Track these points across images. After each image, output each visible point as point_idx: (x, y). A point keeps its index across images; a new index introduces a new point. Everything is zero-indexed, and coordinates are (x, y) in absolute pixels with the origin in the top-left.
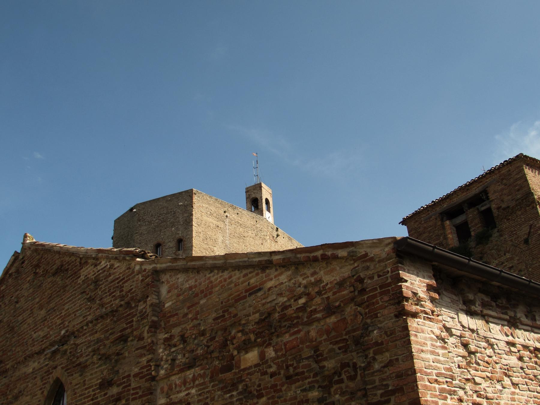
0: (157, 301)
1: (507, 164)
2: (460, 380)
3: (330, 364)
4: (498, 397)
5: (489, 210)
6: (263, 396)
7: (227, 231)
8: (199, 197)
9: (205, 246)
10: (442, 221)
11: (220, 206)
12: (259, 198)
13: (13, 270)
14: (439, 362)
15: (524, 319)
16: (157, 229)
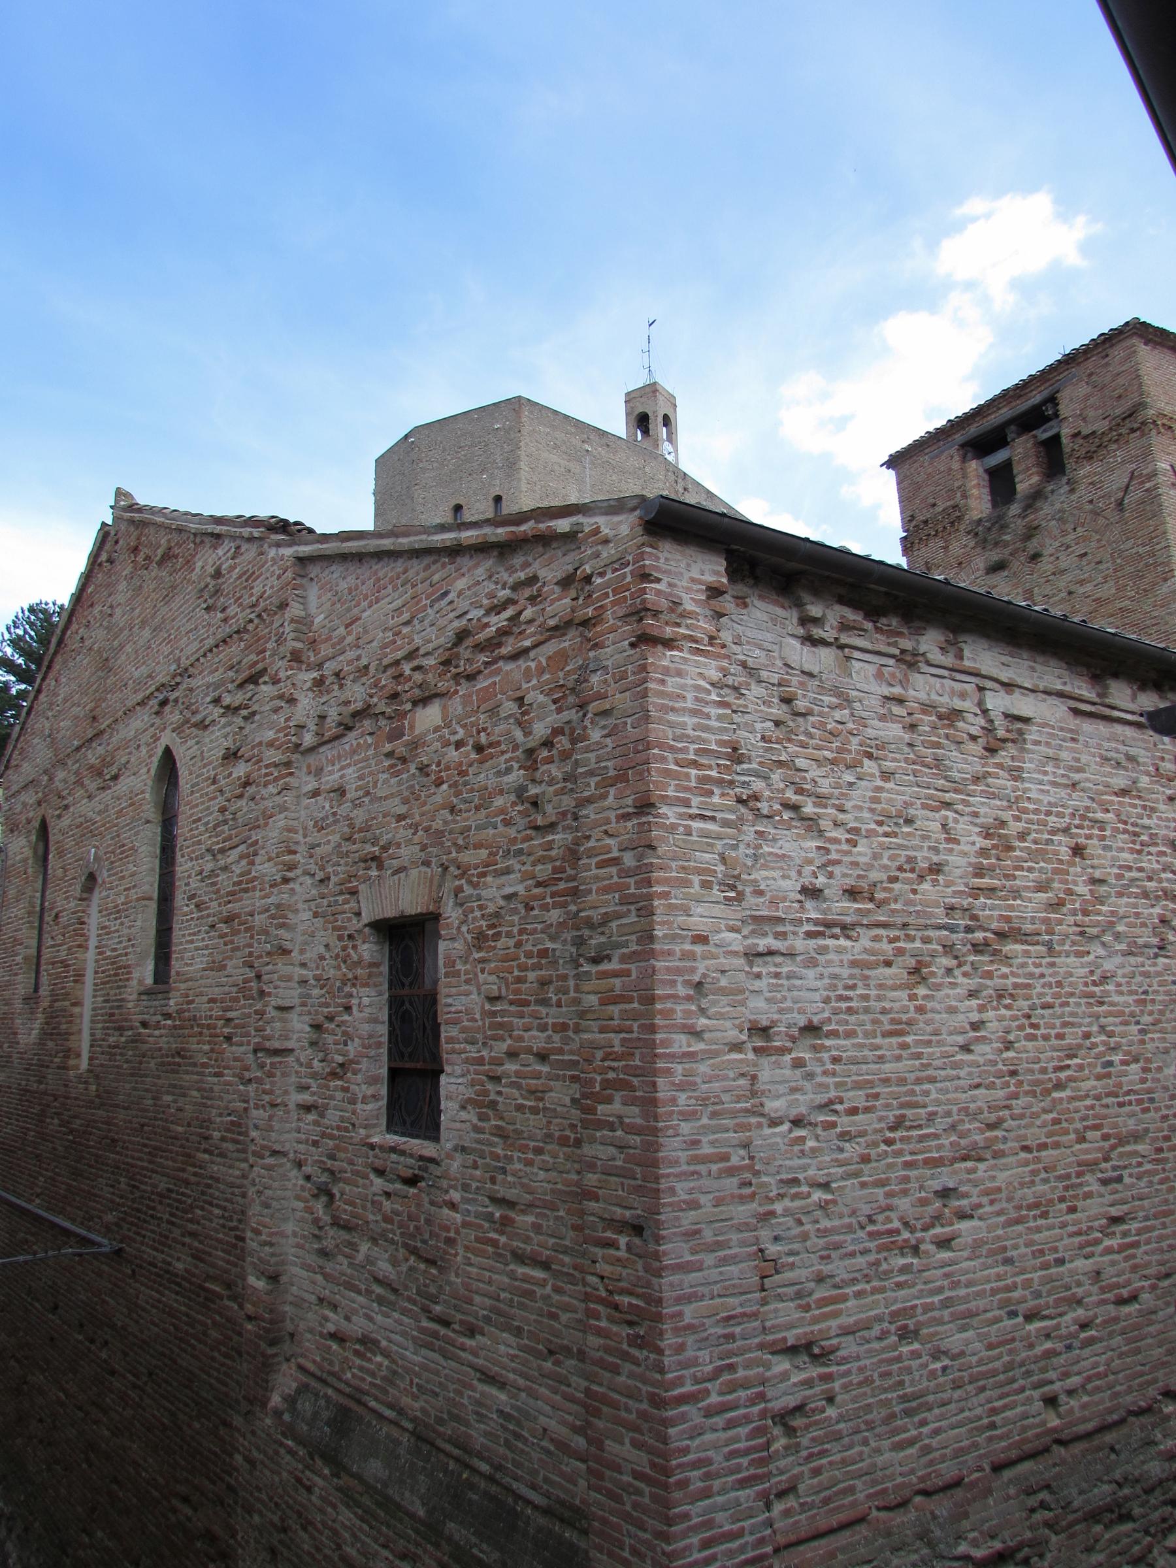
0: (303, 614)
1: (1104, 342)
2: (760, 763)
3: (540, 730)
4: (842, 794)
5: (1056, 438)
6: (443, 783)
10: (964, 459)
13: (104, 557)
14: (707, 729)
15: (936, 656)
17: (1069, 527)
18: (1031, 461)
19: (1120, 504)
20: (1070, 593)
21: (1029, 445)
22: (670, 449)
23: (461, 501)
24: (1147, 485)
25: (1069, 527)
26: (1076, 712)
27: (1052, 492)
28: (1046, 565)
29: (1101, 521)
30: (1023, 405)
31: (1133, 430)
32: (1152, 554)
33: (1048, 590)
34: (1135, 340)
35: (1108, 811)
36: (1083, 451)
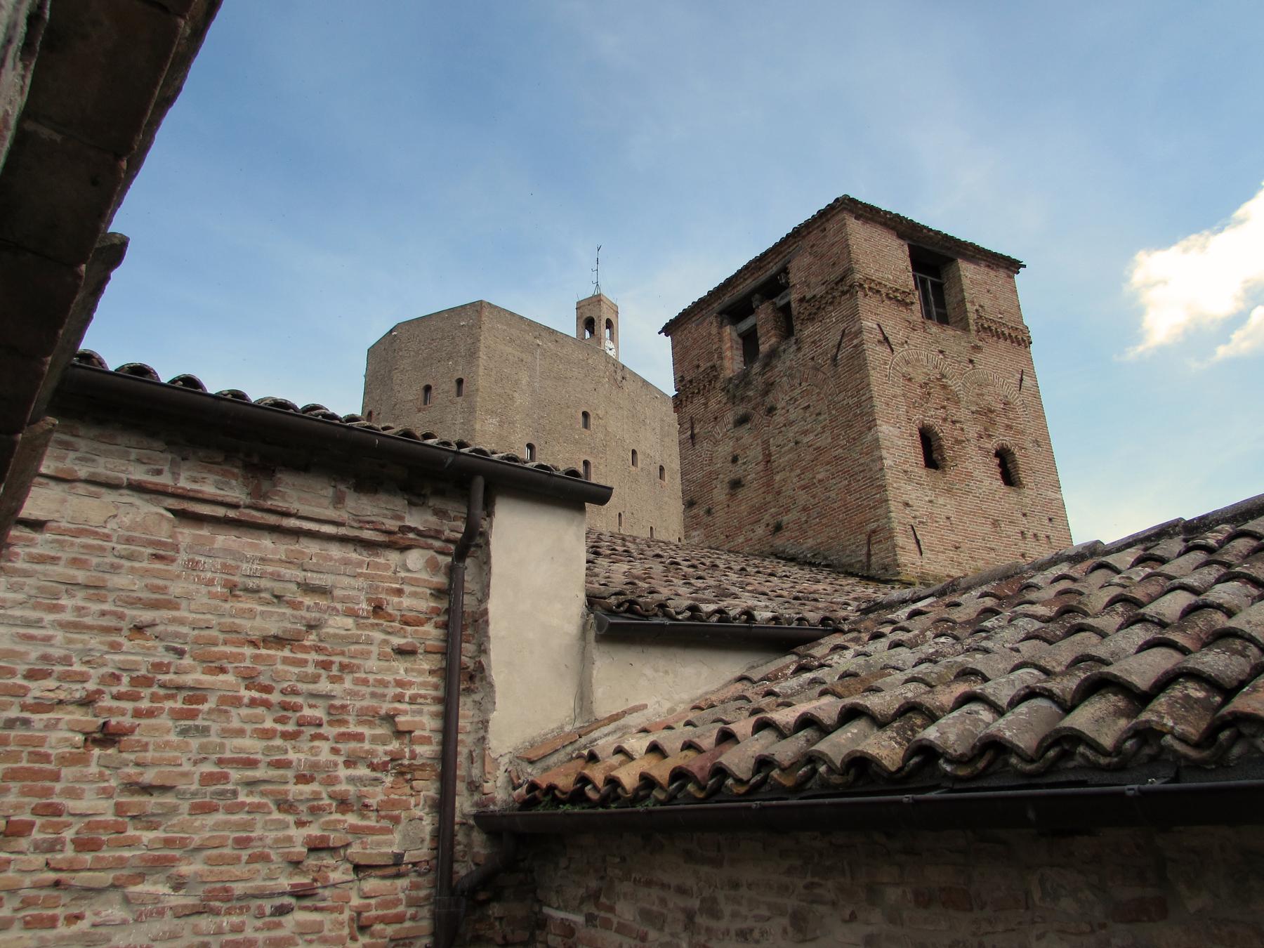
5: (788, 304)
7: (538, 368)
8: (492, 313)
9: (499, 391)
10: (721, 326)
16: (426, 363)
17: (796, 382)
18: (770, 325)
19: (834, 359)
20: (797, 443)
21: (769, 311)
22: (612, 346)
23: (431, 382)
24: (855, 342)
25: (796, 382)
26: (181, 515)
27: (784, 351)
28: (779, 418)
29: (821, 376)
30: (763, 276)
31: (844, 293)
32: (859, 405)
33: (780, 440)
34: (845, 215)
35: (223, 670)
36: (807, 313)
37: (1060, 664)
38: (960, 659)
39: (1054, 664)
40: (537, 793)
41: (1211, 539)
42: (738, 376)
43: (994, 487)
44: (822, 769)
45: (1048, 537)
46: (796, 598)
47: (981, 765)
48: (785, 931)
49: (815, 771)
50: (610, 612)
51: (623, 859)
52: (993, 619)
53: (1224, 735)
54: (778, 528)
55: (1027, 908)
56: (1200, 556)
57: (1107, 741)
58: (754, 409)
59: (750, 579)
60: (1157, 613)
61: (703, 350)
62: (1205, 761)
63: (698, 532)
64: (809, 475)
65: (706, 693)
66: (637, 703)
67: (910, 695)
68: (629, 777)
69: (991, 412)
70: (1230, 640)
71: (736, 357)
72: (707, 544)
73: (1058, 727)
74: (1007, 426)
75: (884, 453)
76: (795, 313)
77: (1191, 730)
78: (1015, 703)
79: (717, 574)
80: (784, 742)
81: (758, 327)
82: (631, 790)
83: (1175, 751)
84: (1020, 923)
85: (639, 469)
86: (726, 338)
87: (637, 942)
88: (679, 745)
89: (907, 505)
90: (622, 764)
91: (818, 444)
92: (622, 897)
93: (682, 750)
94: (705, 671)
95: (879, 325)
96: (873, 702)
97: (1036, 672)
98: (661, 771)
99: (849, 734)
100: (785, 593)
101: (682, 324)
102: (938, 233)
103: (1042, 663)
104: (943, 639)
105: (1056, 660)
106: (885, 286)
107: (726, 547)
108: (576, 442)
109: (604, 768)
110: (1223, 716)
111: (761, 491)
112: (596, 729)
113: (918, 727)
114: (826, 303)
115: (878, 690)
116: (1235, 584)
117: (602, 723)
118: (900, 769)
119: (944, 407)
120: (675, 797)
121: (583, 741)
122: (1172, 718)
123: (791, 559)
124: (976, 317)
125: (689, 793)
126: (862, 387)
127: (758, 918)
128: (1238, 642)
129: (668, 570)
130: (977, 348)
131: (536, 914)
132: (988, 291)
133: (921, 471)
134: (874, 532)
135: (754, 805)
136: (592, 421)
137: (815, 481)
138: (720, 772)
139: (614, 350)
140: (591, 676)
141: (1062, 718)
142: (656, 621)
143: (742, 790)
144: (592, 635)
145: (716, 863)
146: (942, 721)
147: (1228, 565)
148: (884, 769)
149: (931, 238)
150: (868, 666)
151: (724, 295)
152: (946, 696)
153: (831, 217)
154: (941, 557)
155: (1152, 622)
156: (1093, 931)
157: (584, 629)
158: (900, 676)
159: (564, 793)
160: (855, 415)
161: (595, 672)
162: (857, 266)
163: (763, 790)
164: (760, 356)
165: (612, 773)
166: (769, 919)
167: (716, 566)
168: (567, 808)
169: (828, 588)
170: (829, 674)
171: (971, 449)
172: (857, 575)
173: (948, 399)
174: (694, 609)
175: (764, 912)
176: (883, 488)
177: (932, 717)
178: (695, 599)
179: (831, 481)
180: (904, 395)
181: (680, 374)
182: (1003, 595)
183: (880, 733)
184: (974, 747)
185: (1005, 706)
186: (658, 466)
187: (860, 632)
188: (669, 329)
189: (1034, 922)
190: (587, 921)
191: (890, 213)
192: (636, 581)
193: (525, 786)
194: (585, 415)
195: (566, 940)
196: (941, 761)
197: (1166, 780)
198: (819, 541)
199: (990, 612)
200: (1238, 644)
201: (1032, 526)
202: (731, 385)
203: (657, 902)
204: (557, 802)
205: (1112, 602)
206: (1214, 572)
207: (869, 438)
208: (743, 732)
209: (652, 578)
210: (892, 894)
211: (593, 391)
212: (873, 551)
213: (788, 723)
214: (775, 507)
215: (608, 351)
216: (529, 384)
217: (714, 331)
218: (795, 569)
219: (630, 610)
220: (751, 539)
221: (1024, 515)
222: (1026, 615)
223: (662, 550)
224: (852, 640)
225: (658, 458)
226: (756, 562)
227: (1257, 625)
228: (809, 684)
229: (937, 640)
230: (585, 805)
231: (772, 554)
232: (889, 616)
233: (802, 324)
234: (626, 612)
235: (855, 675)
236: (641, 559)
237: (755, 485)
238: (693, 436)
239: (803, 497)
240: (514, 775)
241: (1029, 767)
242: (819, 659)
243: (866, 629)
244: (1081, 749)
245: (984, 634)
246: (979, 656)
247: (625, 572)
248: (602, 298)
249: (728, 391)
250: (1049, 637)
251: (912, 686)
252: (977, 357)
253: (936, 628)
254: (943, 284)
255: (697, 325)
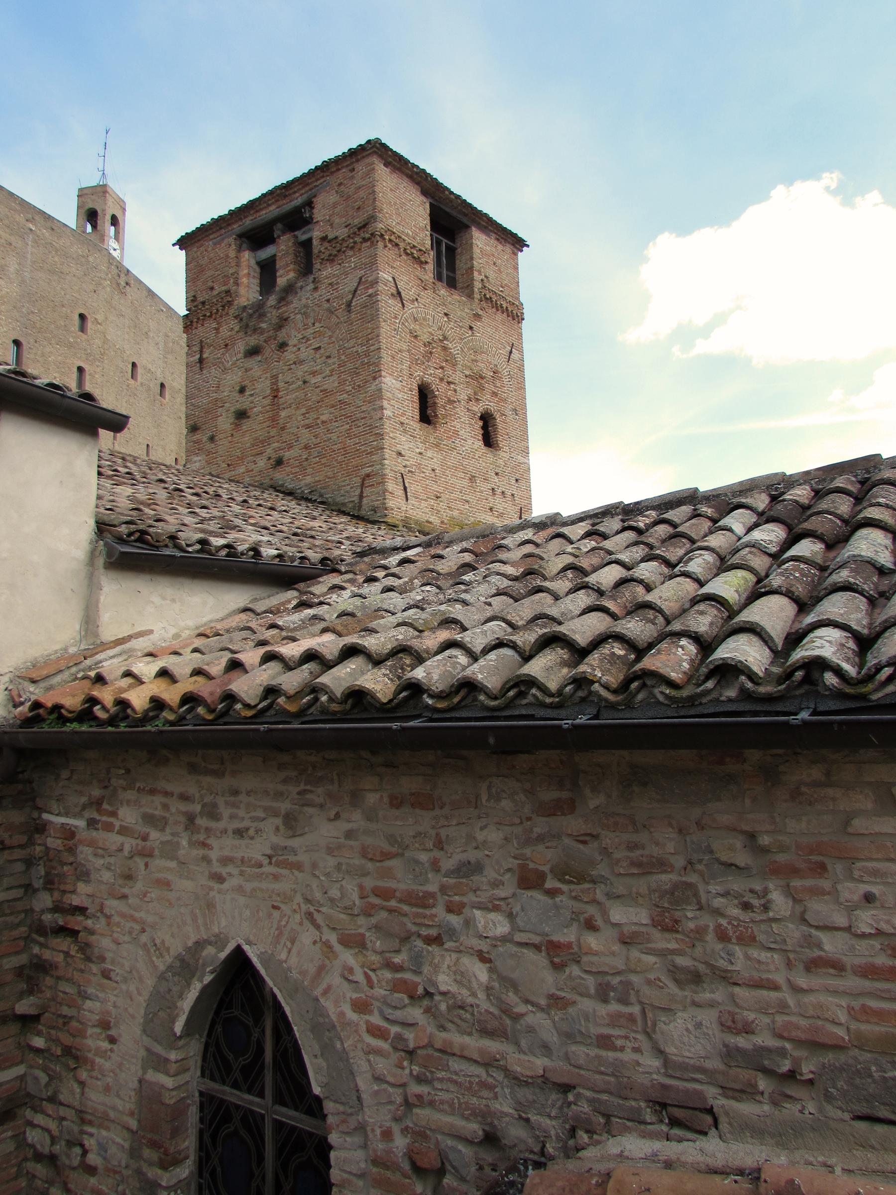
5: (310, 240)
7: (29, 256)
10: (239, 250)
11: (18, 208)
12: (99, 212)
18: (290, 258)
19: (349, 305)
20: (305, 382)
21: (290, 244)
22: (116, 246)
24: (370, 291)
27: (301, 288)
28: (289, 355)
29: (334, 319)
31: (365, 240)
32: (367, 354)
34: (375, 159)
36: (327, 253)
37: (522, 619)
38: (443, 607)
39: (518, 618)
40: (41, 711)
41: (641, 522)
42: (253, 305)
43: (475, 447)
44: (324, 698)
45: (513, 495)
46: (295, 534)
47: (456, 700)
48: (277, 829)
49: (316, 699)
50: (121, 540)
51: (128, 771)
52: (471, 574)
53: (634, 685)
54: (279, 462)
55: (476, 807)
56: (630, 535)
57: (553, 686)
58: (265, 341)
59: (251, 512)
60: (598, 582)
61: (219, 272)
62: (618, 703)
63: (199, 458)
64: (313, 415)
65: (211, 621)
66: (143, 629)
67: (400, 637)
68: (139, 699)
69: (482, 378)
70: (647, 610)
71: (252, 286)
72: (207, 471)
73: (518, 673)
74: (494, 393)
75: (385, 404)
76: (315, 251)
77: (612, 680)
78: (486, 651)
79: (220, 504)
80: (290, 673)
81: (277, 258)
82: (141, 711)
83: (600, 695)
84: (469, 818)
85: (139, 383)
86: (244, 264)
87: (139, 841)
88: (188, 670)
89: (400, 454)
90: (131, 687)
91: (325, 387)
92: (125, 803)
93: (192, 675)
94: (211, 601)
95: (393, 278)
96: (371, 642)
97: (503, 624)
98: (172, 695)
99: (348, 669)
100: (285, 528)
101: (199, 240)
102: (458, 197)
103: (509, 617)
104: (428, 588)
105: (519, 615)
106: (404, 240)
107: (227, 476)
108: (71, 346)
109: (113, 691)
110: (636, 671)
111: (265, 425)
112: (102, 652)
113: (408, 666)
114: (347, 247)
115: (373, 631)
116: (655, 563)
117: (108, 646)
118: (391, 701)
119: (442, 368)
120: (184, 718)
121: (88, 662)
122: (601, 670)
123: (290, 493)
124: (480, 286)
125: (198, 715)
126: (372, 337)
127: (254, 819)
128: (651, 612)
129: (171, 497)
130: (477, 317)
131: (34, 819)
132: (494, 264)
133: (415, 425)
134: (368, 476)
135: (261, 727)
136: (90, 325)
137: (319, 422)
138: (230, 698)
139: (118, 251)
140: (97, 601)
141: (521, 666)
142: (167, 552)
143: (249, 713)
144: (100, 561)
145: (218, 774)
146: (428, 663)
147: (651, 547)
148: (377, 700)
149: (451, 201)
150: (364, 607)
151: (245, 217)
152: (431, 641)
153: (363, 157)
154: (424, 504)
155: (593, 589)
156: (521, 823)
157: (92, 555)
158: (392, 620)
159: (71, 712)
160: (363, 364)
161: (102, 598)
162: (381, 215)
163: (268, 714)
164: (277, 289)
165: (122, 696)
166: (264, 819)
167: (219, 496)
168: (75, 726)
169: (324, 526)
170: (328, 612)
171: (461, 410)
172: (348, 514)
173: (447, 361)
174: (203, 542)
175: (261, 814)
176: (380, 436)
177: (419, 659)
178: (203, 531)
179: (334, 424)
180: (409, 351)
181: (192, 293)
182: (479, 552)
183: (375, 670)
184: (452, 686)
185: (478, 652)
186: (159, 383)
187: (355, 574)
188: (184, 242)
189: (479, 817)
190: (88, 825)
191: (417, 167)
192: (141, 507)
193: (28, 704)
194: (82, 317)
195: (66, 842)
196: (425, 696)
197: (589, 717)
198: (317, 479)
199: (469, 567)
200: (651, 614)
201: (501, 484)
202: (245, 314)
203: (159, 807)
204: (63, 720)
205: (565, 569)
206: (639, 552)
207: (373, 387)
208: (251, 662)
209: (157, 505)
210: (371, 798)
211: (92, 293)
212: (367, 492)
213: (293, 656)
214: (278, 442)
215: (112, 251)
216: (17, 272)
217: (232, 254)
218: (293, 504)
219: (140, 540)
220: (252, 470)
221: (497, 474)
222: (498, 574)
223: (165, 474)
224: (349, 581)
225: (159, 374)
226: (257, 493)
227: (666, 600)
228: (310, 619)
229: (423, 588)
230: (93, 723)
231: (271, 487)
232: (382, 562)
233: (321, 263)
234: (136, 541)
235: (352, 615)
236: (144, 483)
237: (261, 418)
238: (201, 361)
239: (306, 436)
240: (15, 693)
241: (493, 703)
242: (319, 597)
243: (362, 572)
244: (534, 691)
245: (463, 587)
246: (458, 606)
247: (129, 496)
248: (109, 190)
249: (241, 320)
250: (514, 594)
251: (403, 629)
252: (477, 325)
253: (423, 577)
254: (456, 249)
255: (215, 244)
